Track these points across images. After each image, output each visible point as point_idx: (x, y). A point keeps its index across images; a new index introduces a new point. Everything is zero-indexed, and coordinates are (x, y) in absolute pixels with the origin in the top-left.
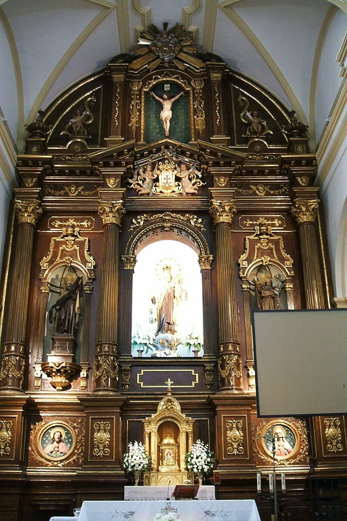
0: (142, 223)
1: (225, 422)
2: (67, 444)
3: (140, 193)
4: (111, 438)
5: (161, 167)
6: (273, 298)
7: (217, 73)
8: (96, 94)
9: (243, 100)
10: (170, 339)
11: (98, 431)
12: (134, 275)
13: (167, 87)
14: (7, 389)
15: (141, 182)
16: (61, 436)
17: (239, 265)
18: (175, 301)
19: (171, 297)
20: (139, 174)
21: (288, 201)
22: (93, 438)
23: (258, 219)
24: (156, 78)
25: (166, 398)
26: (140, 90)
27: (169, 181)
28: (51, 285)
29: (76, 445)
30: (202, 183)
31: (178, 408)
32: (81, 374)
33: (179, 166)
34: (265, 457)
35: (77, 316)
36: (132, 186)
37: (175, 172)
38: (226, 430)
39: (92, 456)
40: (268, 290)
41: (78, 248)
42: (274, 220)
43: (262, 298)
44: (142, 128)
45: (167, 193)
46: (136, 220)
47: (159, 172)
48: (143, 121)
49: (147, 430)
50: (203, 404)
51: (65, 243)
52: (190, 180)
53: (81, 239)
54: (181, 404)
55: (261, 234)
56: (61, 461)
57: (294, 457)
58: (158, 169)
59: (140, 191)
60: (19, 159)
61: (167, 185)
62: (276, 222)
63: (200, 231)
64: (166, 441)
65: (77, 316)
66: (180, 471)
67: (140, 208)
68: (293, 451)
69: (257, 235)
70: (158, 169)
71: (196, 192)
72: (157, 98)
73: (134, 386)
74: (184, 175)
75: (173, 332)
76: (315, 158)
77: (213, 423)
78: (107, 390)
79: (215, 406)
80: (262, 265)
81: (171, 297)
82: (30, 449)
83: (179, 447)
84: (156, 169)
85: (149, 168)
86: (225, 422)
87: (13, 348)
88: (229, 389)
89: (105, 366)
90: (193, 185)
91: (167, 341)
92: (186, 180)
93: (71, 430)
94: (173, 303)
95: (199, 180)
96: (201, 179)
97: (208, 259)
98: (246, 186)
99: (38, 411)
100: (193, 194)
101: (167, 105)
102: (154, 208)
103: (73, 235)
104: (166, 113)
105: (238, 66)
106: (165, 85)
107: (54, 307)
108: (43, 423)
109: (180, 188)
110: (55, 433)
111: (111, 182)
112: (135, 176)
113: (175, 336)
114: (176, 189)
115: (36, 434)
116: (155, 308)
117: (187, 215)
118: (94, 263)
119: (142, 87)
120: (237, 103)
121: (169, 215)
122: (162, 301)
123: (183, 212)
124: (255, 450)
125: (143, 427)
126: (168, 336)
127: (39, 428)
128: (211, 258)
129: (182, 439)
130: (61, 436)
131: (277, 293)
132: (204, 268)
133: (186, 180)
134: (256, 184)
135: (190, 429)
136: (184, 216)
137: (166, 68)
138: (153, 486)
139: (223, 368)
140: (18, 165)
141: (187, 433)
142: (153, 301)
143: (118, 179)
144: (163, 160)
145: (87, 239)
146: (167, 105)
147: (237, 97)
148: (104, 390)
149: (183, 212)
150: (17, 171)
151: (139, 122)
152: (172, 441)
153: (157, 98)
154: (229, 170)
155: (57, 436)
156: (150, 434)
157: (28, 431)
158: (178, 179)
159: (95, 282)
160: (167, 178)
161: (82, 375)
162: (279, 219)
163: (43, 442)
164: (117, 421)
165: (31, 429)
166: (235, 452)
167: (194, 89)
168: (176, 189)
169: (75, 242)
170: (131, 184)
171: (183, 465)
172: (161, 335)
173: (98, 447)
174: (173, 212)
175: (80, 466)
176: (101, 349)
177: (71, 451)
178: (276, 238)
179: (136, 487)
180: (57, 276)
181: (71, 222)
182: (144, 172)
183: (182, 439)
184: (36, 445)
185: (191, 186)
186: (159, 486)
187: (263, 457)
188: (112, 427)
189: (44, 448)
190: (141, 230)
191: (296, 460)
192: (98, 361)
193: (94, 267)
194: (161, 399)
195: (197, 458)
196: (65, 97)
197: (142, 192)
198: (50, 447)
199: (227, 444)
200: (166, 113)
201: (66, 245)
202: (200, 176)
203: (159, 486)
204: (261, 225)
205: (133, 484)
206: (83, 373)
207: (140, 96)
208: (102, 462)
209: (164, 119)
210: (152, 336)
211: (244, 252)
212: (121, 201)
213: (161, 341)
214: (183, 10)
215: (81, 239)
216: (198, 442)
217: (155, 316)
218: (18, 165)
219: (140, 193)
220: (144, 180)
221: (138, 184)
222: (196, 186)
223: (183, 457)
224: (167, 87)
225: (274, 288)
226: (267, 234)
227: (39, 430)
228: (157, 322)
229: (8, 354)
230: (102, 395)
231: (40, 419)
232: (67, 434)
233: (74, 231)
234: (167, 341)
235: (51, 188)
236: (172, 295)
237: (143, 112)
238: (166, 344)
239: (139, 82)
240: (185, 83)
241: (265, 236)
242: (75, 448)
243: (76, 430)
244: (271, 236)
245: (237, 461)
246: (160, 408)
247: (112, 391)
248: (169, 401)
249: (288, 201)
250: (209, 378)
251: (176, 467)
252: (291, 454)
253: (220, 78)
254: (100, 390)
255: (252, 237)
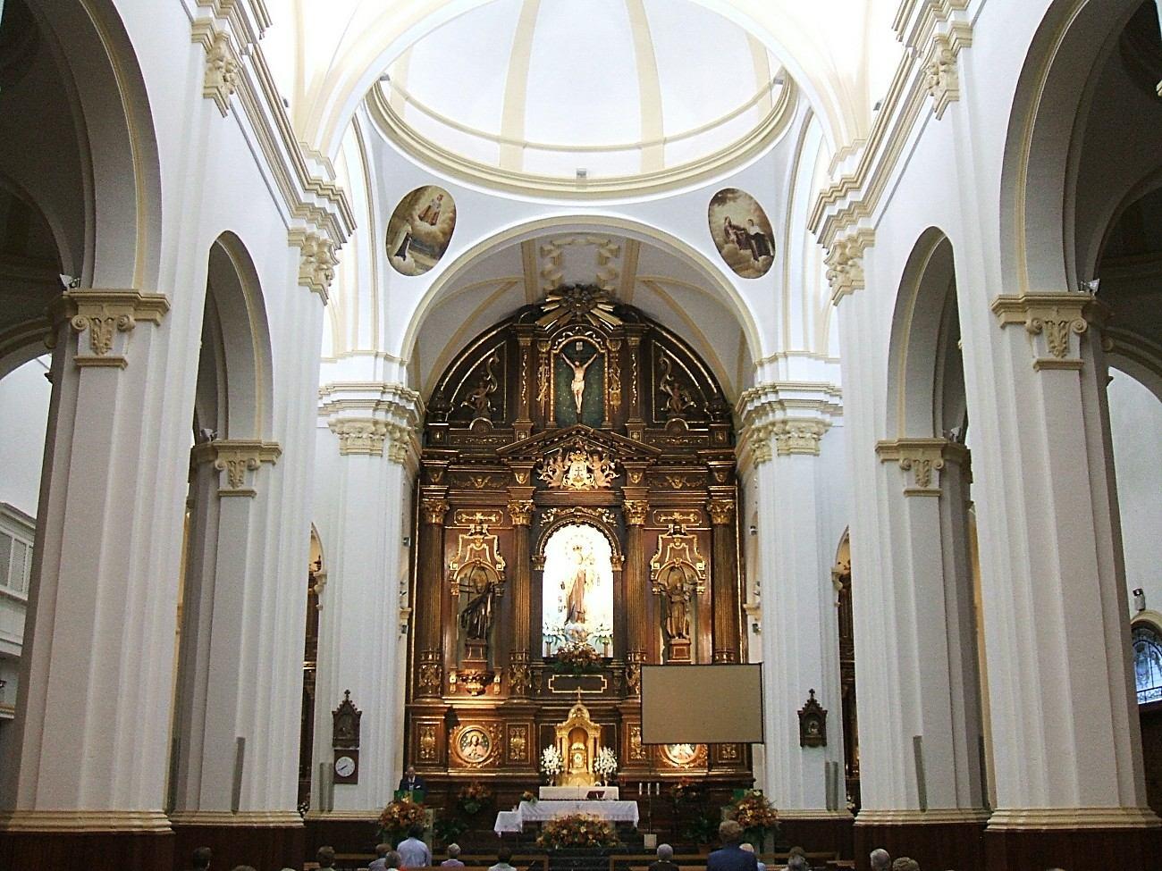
0: (552, 518)
1: (630, 729)
2: (483, 747)
3: (550, 486)
4: (526, 743)
5: (572, 457)
6: (683, 604)
7: (636, 336)
8: (499, 352)
9: (665, 362)
10: (580, 629)
11: (515, 737)
12: (544, 574)
13: (579, 346)
14: (427, 697)
15: (551, 473)
16: (478, 739)
17: (651, 566)
18: (585, 586)
19: (581, 581)
20: (548, 465)
21: (705, 496)
22: (509, 742)
23: (672, 514)
24: (568, 336)
25: (576, 707)
26: (549, 352)
27: (580, 473)
28: (461, 585)
29: (493, 748)
30: (615, 475)
31: (587, 715)
32: (495, 679)
33: (592, 457)
34: (668, 761)
35: (489, 619)
36: (542, 477)
37: (588, 463)
38: (630, 736)
39: (510, 760)
40: (679, 595)
41: (487, 548)
42: (689, 516)
43: (672, 603)
44: (552, 402)
45: (578, 485)
46: (546, 515)
47: (569, 464)
48: (552, 391)
49: (559, 735)
50: (610, 710)
51: (473, 541)
52: (603, 471)
53: (490, 537)
54: (588, 710)
55: (675, 533)
56: (479, 763)
57: (694, 761)
58: (570, 460)
59: (550, 483)
60: (424, 453)
61: (578, 478)
62: (691, 517)
63: (612, 527)
64: (575, 746)
65: (489, 619)
66: (588, 773)
67: (552, 503)
68: (693, 755)
69: (670, 534)
70: (570, 460)
71: (609, 485)
72: (568, 362)
73: (546, 692)
74: (597, 466)
75: (584, 621)
76: (733, 454)
77: (619, 728)
78: (522, 698)
79: (621, 715)
80: (674, 567)
81: (581, 581)
82: (449, 752)
83: (587, 751)
84: (567, 460)
85: (559, 459)
86: (630, 729)
87: (430, 657)
88: (634, 698)
89: (519, 675)
90: (607, 476)
91: (577, 632)
92: (598, 473)
93: (487, 734)
94: (584, 589)
95: (612, 472)
96: (613, 470)
97: (619, 559)
98: (661, 477)
99: (456, 716)
100: (606, 487)
101: (579, 374)
102: (564, 503)
103: (481, 533)
104: (578, 385)
105: (658, 318)
106: (577, 344)
107: (466, 611)
108: (461, 728)
109: (592, 479)
110: (473, 737)
111: (520, 479)
112: (545, 467)
113: (586, 626)
114: (587, 482)
115: (455, 738)
116: (565, 594)
117: (599, 509)
118: (504, 564)
119: (551, 349)
120: (657, 365)
121: (580, 511)
122: (572, 586)
123: (594, 507)
124: (658, 754)
125: (555, 733)
126: (578, 626)
127: (459, 731)
128: (623, 559)
129: (591, 744)
130: (478, 739)
131: (687, 598)
132: (615, 569)
133: (598, 473)
134: (672, 475)
135: (598, 735)
136: (595, 511)
137: (579, 322)
138: (564, 786)
139: (630, 677)
140: (423, 458)
141: (595, 739)
142: (563, 586)
143: (527, 475)
144: (573, 449)
145: (496, 537)
146: (579, 374)
147: (658, 357)
148: (519, 698)
149: (594, 507)
150: (421, 464)
151: (547, 395)
152: (582, 746)
153: (568, 362)
154: (642, 465)
155: (474, 740)
156: (561, 739)
157: (448, 734)
158: (590, 471)
159: (505, 585)
160: (578, 470)
161: (495, 681)
162: (695, 513)
163: (462, 746)
164: (532, 727)
165: (450, 734)
166: (639, 757)
167: (609, 351)
168: (587, 482)
169: (485, 541)
170: (541, 475)
171: (591, 769)
172: (571, 625)
173: (515, 751)
174: (584, 507)
175: (498, 767)
176: (514, 657)
177: (488, 754)
178: (691, 536)
179: (550, 787)
180: (466, 575)
181: (479, 516)
182: (554, 463)
183: (591, 744)
184: (455, 748)
185: (604, 478)
186: (570, 787)
187: (666, 760)
188: (527, 733)
189: (462, 751)
190: (550, 527)
191: (696, 764)
192: (512, 669)
193: (505, 568)
194: (572, 705)
195: (550, 762)
196: (464, 357)
197: (552, 485)
198: (468, 750)
199: (630, 749)
200: (578, 385)
201: (475, 543)
202: (613, 467)
203: (570, 787)
204: (675, 522)
205: (548, 784)
206: (497, 679)
207: (549, 361)
208: (518, 765)
209: (575, 392)
210: (561, 626)
211: (657, 553)
212: (532, 501)
213: (571, 632)
214: (597, 276)
215: (490, 537)
216: (605, 748)
217: (564, 603)
218: (423, 458)
219: (550, 486)
220: (554, 472)
221: (549, 476)
222: (608, 479)
223: (591, 761)
224: (579, 346)
225: (685, 593)
226: (681, 534)
227: (457, 734)
228: (566, 609)
229: (426, 662)
230: (516, 704)
231: (458, 724)
232: (483, 737)
233: (482, 529)
234: (577, 632)
235: (456, 478)
236: (583, 580)
237: (552, 381)
238: (576, 635)
239: (547, 341)
240: (599, 343)
241: (678, 536)
242: (492, 751)
243: (493, 735)
244: (685, 534)
245: (640, 765)
246: (571, 715)
247: (526, 699)
248: (579, 709)
249: (705, 496)
250: (617, 684)
251: (584, 770)
252: (692, 758)
253: (638, 343)
254: (514, 698)
255: (665, 536)
